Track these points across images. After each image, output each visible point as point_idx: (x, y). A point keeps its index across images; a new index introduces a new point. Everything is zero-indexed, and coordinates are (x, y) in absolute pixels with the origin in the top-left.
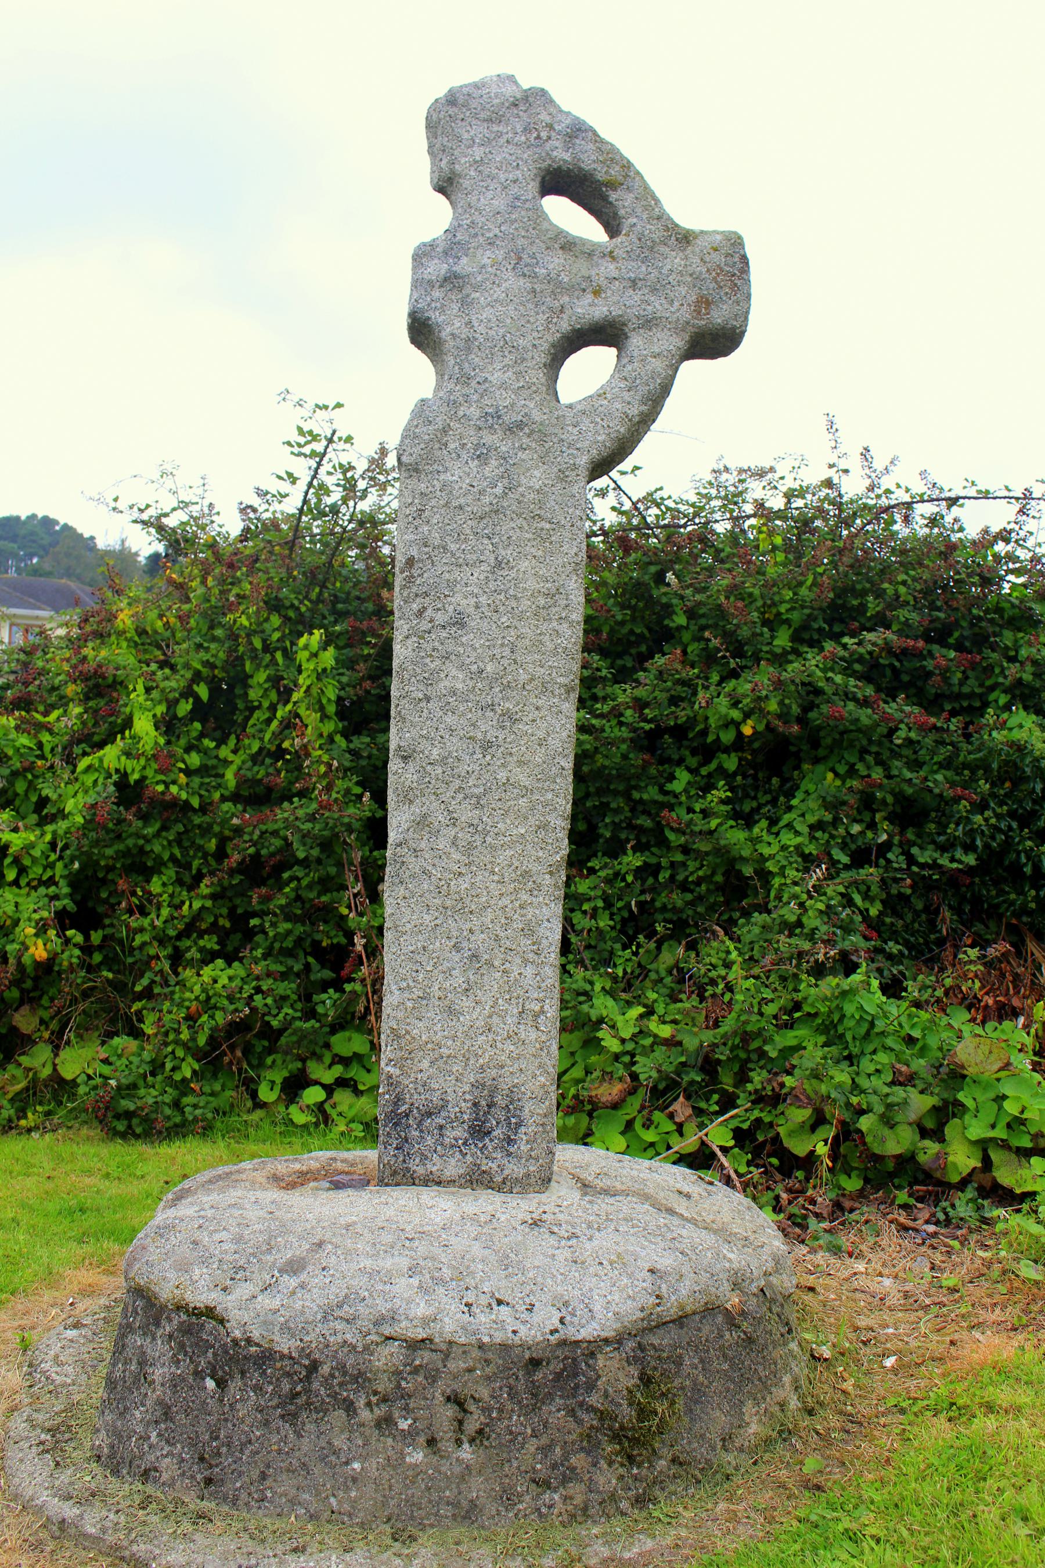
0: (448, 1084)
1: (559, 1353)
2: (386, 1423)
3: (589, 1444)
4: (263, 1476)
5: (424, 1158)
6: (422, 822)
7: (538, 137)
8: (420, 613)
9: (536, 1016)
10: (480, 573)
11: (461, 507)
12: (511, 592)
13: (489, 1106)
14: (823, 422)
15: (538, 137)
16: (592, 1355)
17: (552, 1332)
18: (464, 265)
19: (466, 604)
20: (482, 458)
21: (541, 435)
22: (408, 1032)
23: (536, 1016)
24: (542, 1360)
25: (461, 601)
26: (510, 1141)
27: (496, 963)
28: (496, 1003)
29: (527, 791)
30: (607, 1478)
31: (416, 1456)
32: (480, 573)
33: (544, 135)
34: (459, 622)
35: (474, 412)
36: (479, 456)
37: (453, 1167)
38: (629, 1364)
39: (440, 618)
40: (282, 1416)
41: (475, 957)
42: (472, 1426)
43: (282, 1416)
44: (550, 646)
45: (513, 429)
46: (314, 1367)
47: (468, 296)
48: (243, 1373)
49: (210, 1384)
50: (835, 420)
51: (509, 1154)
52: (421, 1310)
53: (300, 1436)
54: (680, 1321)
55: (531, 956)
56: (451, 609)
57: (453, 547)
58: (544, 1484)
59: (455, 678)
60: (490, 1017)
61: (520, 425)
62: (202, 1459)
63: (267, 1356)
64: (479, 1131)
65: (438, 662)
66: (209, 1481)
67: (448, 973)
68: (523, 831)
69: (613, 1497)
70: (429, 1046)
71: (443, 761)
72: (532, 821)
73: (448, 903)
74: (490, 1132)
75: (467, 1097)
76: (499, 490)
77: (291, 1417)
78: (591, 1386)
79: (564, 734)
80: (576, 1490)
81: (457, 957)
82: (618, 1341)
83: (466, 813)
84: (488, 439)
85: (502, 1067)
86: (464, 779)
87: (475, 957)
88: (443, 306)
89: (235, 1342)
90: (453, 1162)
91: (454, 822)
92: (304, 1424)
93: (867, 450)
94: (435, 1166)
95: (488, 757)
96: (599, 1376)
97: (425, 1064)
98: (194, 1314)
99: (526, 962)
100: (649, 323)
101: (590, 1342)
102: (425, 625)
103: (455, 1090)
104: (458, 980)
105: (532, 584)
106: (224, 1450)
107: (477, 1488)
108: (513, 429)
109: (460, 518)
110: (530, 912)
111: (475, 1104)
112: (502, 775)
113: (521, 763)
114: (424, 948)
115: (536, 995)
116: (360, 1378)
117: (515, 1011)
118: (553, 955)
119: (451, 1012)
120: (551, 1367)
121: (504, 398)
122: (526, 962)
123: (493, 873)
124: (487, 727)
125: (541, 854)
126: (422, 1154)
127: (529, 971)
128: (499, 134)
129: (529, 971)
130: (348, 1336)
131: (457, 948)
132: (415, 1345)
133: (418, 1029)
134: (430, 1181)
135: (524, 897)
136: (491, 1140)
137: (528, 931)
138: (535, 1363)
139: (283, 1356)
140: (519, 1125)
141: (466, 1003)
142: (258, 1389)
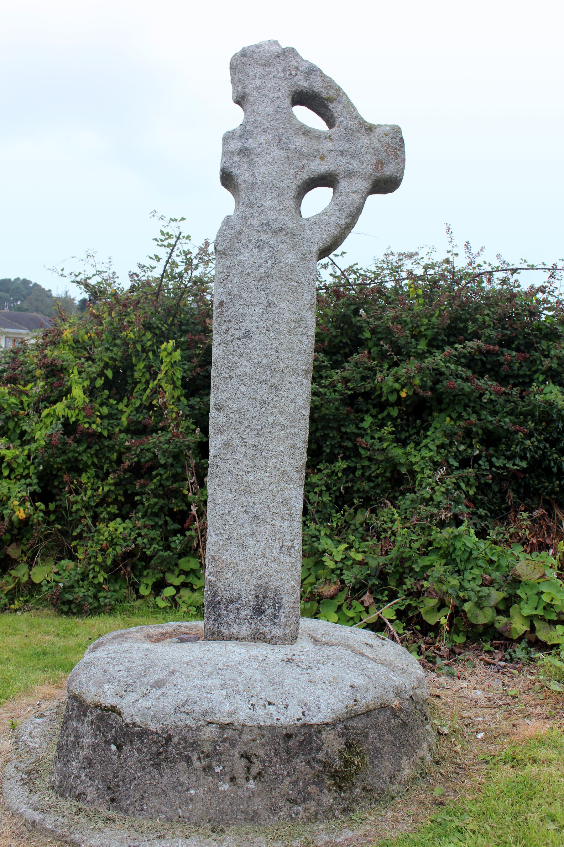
0: (242, 585)
1: (302, 731)
2: (208, 769)
3: (318, 780)
4: (142, 797)
5: (229, 625)
6: (228, 444)
7: (290, 74)
8: (227, 331)
9: (289, 549)
10: (259, 310)
11: (249, 274)
12: (276, 320)
13: (264, 598)
14: (444, 228)
15: (290, 74)
16: (320, 732)
17: (298, 720)
18: (251, 143)
19: (252, 326)
20: (260, 247)
21: (292, 235)
22: (220, 558)
23: (289, 549)
24: (293, 735)
25: (249, 325)
26: (275, 616)
27: (268, 520)
28: (268, 542)
29: (285, 427)
30: (328, 799)
31: (225, 787)
32: (259, 310)
33: (294, 73)
34: (248, 336)
35: (256, 222)
36: (258, 247)
37: (245, 631)
38: (340, 737)
39: (238, 334)
40: (152, 765)
41: (256, 517)
42: (255, 770)
43: (152, 765)
44: (297, 349)
45: (277, 232)
46: (169, 738)
47: (252, 160)
48: (131, 742)
49: (113, 747)
50: (451, 227)
51: (275, 624)
52: (227, 707)
53: (162, 776)
54: (367, 713)
55: (287, 516)
56: (243, 329)
57: (244, 295)
58: (293, 802)
59: (246, 366)
60: (265, 549)
61: (281, 230)
62: (109, 788)
63: (144, 733)
64: (258, 611)
65: (236, 358)
66: (113, 800)
67: (242, 526)
68: (282, 449)
69: (331, 809)
70: (232, 565)
71: (239, 411)
72: (287, 443)
73: (242, 488)
74: (264, 612)
75: (252, 592)
76: (269, 265)
77: (157, 766)
78: (319, 749)
79: (305, 397)
80: (311, 805)
81: (246, 517)
82: (333, 725)
83: (252, 439)
84: (264, 237)
85: (271, 576)
86: (250, 421)
87: (256, 517)
88: (239, 165)
89: (127, 725)
90: (244, 627)
91: (245, 444)
92: (164, 769)
93: (468, 243)
94: (235, 630)
95: (264, 409)
96: (323, 744)
97: (230, 575)
98: (105, 710)
99: (284, 519)
100: (350, 174)
101: (318, 725)
102: (229, 338)
103: (246, 589)
104: (247, 529)
105: (287, 315)
106: (121, 783)
107: (258, 804)
108: (277, 232)
109: (248, 280)
110: (286, 493)
111: (256, 597)
112: (271, 419)
113: (281, 412)
114: (229, 512)
115: (289, 538)
116: (194, 745)
117: (278, 546)
118: (298, 516)
119: (244, 546)
120: (297, 739)
121: (272, 215)
122: (284, 519)
123: (266, 471)
124: (263, 393)
125: (292, 461)
126: (228, 624)
127: (286, 524)
128: (270, 72)
129: (286, 524)
130: (188, 722)
131: (247, 512)
132: (224, 727)
133: (226, 556)
134: (232, 638)
135: (283, 484)
136: (265, 616)
137: (285, 503)
138: (289, 736)
139: (153, 733)
140: (280, 608)
141: (252, 542)
142: (139, 750)
